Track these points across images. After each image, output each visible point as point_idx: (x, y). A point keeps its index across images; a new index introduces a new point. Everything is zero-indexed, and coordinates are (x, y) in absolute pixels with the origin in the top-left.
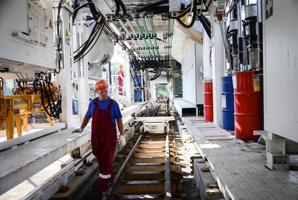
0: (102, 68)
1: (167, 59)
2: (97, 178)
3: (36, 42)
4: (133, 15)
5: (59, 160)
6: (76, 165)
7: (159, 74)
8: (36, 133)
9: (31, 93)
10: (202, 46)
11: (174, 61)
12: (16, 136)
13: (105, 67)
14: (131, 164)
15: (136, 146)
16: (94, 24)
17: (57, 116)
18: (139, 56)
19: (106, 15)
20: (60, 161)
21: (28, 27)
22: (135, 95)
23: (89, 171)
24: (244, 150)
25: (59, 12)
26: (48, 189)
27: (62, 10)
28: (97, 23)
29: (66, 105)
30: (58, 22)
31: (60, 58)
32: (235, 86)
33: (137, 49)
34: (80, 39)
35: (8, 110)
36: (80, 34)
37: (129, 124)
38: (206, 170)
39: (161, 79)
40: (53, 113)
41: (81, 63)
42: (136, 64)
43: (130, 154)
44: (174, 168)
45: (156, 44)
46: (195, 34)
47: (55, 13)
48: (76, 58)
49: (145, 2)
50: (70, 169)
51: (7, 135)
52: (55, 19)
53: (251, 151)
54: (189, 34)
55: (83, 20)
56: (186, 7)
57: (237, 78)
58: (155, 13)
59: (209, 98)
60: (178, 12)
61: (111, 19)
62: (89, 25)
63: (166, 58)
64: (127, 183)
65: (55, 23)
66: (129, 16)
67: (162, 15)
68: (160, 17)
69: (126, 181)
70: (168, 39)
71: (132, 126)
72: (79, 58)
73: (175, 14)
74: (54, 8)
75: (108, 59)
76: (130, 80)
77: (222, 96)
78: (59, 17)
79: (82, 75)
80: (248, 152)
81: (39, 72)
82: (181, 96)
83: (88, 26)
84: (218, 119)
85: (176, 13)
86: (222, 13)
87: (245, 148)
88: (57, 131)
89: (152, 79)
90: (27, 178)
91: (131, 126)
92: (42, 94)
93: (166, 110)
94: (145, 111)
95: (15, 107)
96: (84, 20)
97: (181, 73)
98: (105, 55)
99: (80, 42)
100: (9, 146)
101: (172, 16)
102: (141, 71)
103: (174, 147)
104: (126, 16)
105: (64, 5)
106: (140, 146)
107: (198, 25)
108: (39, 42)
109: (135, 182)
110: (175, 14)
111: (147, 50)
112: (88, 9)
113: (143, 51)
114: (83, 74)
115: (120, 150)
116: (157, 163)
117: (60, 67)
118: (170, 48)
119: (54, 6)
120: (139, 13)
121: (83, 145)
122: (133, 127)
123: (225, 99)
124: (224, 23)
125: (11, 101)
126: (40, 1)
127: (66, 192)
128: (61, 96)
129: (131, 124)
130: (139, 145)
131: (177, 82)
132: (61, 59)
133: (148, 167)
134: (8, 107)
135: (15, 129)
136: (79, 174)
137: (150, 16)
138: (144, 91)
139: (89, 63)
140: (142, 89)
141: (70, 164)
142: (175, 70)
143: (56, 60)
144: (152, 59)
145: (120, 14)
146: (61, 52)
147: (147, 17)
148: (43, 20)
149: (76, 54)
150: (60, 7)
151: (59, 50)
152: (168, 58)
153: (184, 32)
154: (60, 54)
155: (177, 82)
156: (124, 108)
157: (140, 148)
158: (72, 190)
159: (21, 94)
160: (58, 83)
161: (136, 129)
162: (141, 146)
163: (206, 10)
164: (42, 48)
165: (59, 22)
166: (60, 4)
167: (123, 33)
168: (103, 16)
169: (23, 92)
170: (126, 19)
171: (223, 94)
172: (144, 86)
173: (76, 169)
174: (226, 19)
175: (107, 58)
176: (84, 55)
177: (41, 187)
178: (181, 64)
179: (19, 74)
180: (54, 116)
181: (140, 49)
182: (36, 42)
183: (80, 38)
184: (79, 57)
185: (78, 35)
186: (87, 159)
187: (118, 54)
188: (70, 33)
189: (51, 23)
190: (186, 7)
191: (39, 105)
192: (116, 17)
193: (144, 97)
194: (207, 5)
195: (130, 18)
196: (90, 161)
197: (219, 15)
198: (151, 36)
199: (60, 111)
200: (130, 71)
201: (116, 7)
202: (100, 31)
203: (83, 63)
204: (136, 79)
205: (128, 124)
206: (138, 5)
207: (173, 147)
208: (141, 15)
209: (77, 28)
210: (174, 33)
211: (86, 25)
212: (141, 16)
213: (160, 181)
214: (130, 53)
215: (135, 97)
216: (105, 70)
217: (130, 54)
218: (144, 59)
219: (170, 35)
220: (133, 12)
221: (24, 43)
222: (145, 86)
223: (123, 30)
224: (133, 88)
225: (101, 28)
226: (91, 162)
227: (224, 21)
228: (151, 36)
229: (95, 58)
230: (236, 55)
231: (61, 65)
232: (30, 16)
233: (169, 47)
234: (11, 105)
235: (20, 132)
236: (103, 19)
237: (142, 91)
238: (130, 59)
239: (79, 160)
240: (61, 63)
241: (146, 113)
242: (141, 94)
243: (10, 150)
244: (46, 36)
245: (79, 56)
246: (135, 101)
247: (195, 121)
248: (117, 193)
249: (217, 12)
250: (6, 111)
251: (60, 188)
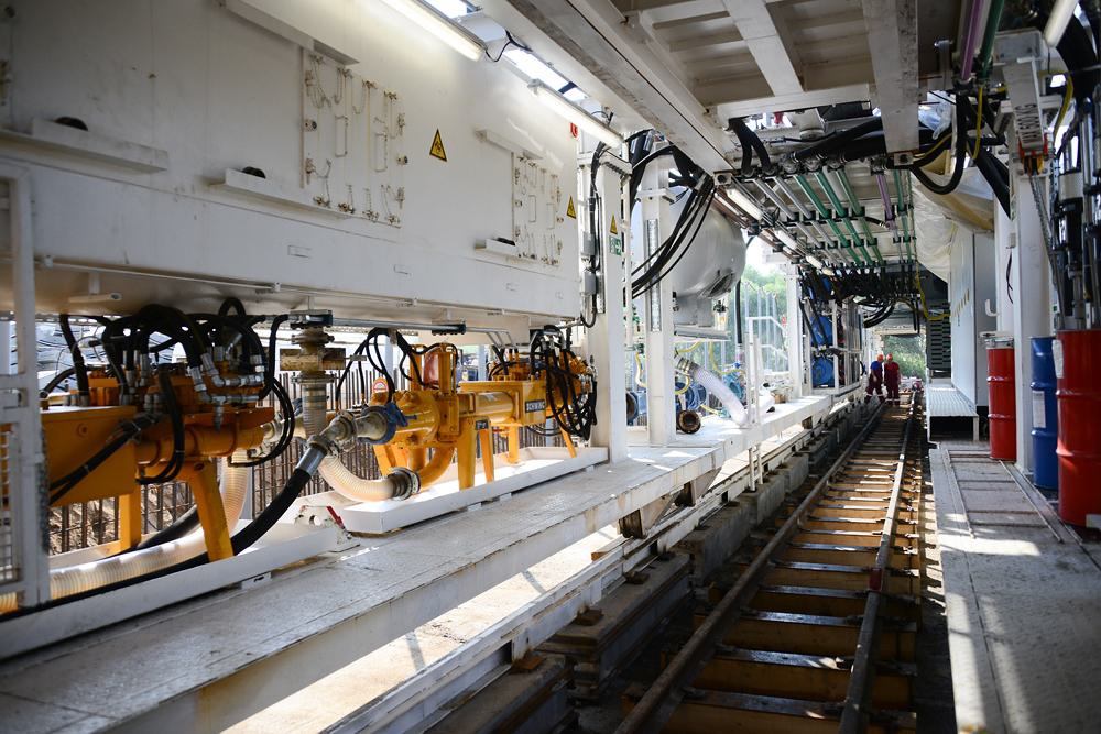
0: (714, 303)
1: (907, 269)
2: (683, 594)
3: (533, 257)
4: (789, 168)
5: (602, 530)
6: (626, 557)
7: (888, 309)
8: (528, 475)
9: (524, 378)
10: (990, 240)
11: (927, 273)
12: (480, 479)
13: (721, 299)
14: (778, 563)
15: (803, 512)
16: (688, 195)
17: (585, 434)
18: (824, 265)
19: (715, 173)
20: (604, 535)
21: (513, 220)
22: (813, 368)
23: (660, 575)
24: (1064, 566)
25: (593, 177)
26: (548, 616)
27: (600, 171)
28: (695, 192)
29: (609, 404)
30: (593, 201)
31: (597, 287)
32: (1059, 373)
33: (816, 248)
34: (653, 236)
35: (462, 420)
36: (653, 222)
37: (793, 449)
39: (899, 324)
40: (573, 425)
41: (655, 295)
42: (812, 284)
43: (780, 534)
44: (893, 586)
45: (868, 232)
46: (971, 206)
47: (583, 182)
48: (637, 285)
49: (821, 131)
50: (611, 566)
51: (460, 478)
52: (582, 194)
53: (1086, 571)
54: (952, 208)
55: (660, 188)
56: (935, 137)
57: (1064, 347)
58: (851, 158)
59: (1004, 393)
60: (914, 152)
61: (729, 181)
62: (674, 198)
63: (903, 267)
64: (757, 614)
65: (584, 204)
66: (781, 169)
67: (872, 162)
68: (866, 164)
69: (754, 612)
70: (899, 219)
71: (800, 455)
72: (648, 284)
73: (903, 159)
74: (582, 167)
75: (728, 281)
76: (801, 329)
78: (593, 188)
79: (656, 325)
80: (1077, 572)
81: (541, 328)
82: (947, 373)
83: (672, 202)
84: (1027, 457)
86: (1037, 153)
87: (1072, 560)
88: (583, 470)
89: (868, 324)
90: (522, 569)
91: (797, 455)
92: (549, 380)
93: (908, 410)
94: (846, 410)
95: (481, 413)
96: (661, 186)
97: (946, 307)
98: (719, 272)
99: (653, 242)
100: (494, 496)
101: (897, 163)
102: (833, 304)
103: (912, 522)
104: (770, 170)
105: (606, 158)
106: (813, 515)
107: (973, 178)
108: (539, 257)
109: (779, 614)
110: (903, 159)
111: (857, 248)
112: (670, 159)
113: (835, 251)
114: (660, 323)
115: (760, 520)
116: (852, 567)
117: (595, 311)
118: (909, 240)
119: (583, 162)
121: (648, 505)
122: (805, 458)
124: (1048, 181)
125: (471, 398)
126: (7, 427)
127: (591, 625)
128: (595, 384)
129: (797, 449)
130: (811, 511)
132: (597, 290)
133: (823, 575)
134: (465, 413)
135: (479, 466)
136: (632, 579)
137: (838, 165)
138: (841, 358)
139: (674, 295)
140: (835, 351)
141: (611, 554)
142: (932, 299)
143: (586, 294)
144: (863, 271)
145: (756, 166)
146: (598, 274)
147: (830, 169)
148: (550, 201)
149: (641, 273)
150: (595, 165)
151: (593, 269)
152: (910, 267)
153: (939, 203)
154: (597, 278)
156: (777, 407)
157: (810, 518)
158: (609, 622)
159: (502, 379)
160: (589, 352)
161: (814, 463)
162: (817, 512)
163: (1000, 140)
164: (549, 269)
165: (594, 201)
166: (596, 157)
167: (772, 208)
168: (708, 176)
169: (507, 374)
170: (774, 178)
172: (840, 345)
173: (629, 566)
174: (1055, 165)
175: (725, 279)
176: (661, 274)
177: (530, 609)
178: (946, 284)
179: (493, 335)
180: (578, 433)
181: (823, 248)
182: (533, 257)
183: (653, 232)
184: (649, 280)
185: (647, 225)
186: (660, 543)
187: (767, 261)
188: (624, 226)
189: (571, 208)
190: (935, 137)
191: (541, 405)
192: (739, 178)
193: (841, 374)
194: (996, 128)
195: (782, 173)
196: (668, 547)
197: (1027, 158)
198: (850, 213)
199: (592, 419)
200: (802, 306)
201: (741, 149)
202: (704, 208)
203: (659, 296)
204: (816, 326)
205: (790, 449)
206: (803, 140)
207: (907, 523)
208: (811, 164)
209: (643, 207)
210: (915, 204)
211: (668, 199)
212: (810, 167)
213: (850, 622)
214: (798, 259)
215: (814, 375)
216: (722, 309)
217: (798, 262)
218: (839, 272)
219: (905, 210)
220: (789, 159)
221: (502, 261)
222: (846, 343)
223: (769, 203)
224: (809, 349)
225: (707, 201)
226: (672, 550)
227: (1049, 173)
228: (850, 213)
229: (694, 281)
230: (1079, 272)
231: (599, 306)
232: (518, 197)
233: (908, 240)
234: (472, 409)
235: (490, 471)
236: (709, 181)
237: (836, 358)
238: (801, 274)
239: (637, 543)
240: (598, 301)
241: (848, 417)
242: (832, 364)
243: (463, 515)
244: (558, 238)
245: (648, 280)
246: (815, 387)
247: (961, 456)
248: (724, 643)
249: (1022, 150)
250: (458, 424)
251: (579, 614)
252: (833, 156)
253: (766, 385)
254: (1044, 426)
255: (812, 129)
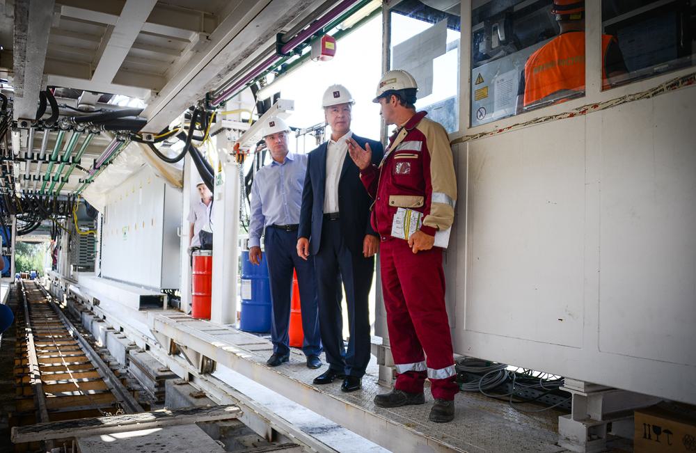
1: (71, 199)
4: (64, 125)
7: (36, 224)
38: (199, 394)
63: (69, 198)
77: (243, 280)
85: (152, 135)
97: (93, 228)
101: (144, 139)
110: (149, 137)
111: (35, 181)
120: (78, 124)
123: (250, 285)
131: (85, 239)
152: (74, 198)
155: (85, 239)
171: (244, 278)
252: (97, 125)
253: (48, 275)
254: (250, 298)
255: (89, 104)
